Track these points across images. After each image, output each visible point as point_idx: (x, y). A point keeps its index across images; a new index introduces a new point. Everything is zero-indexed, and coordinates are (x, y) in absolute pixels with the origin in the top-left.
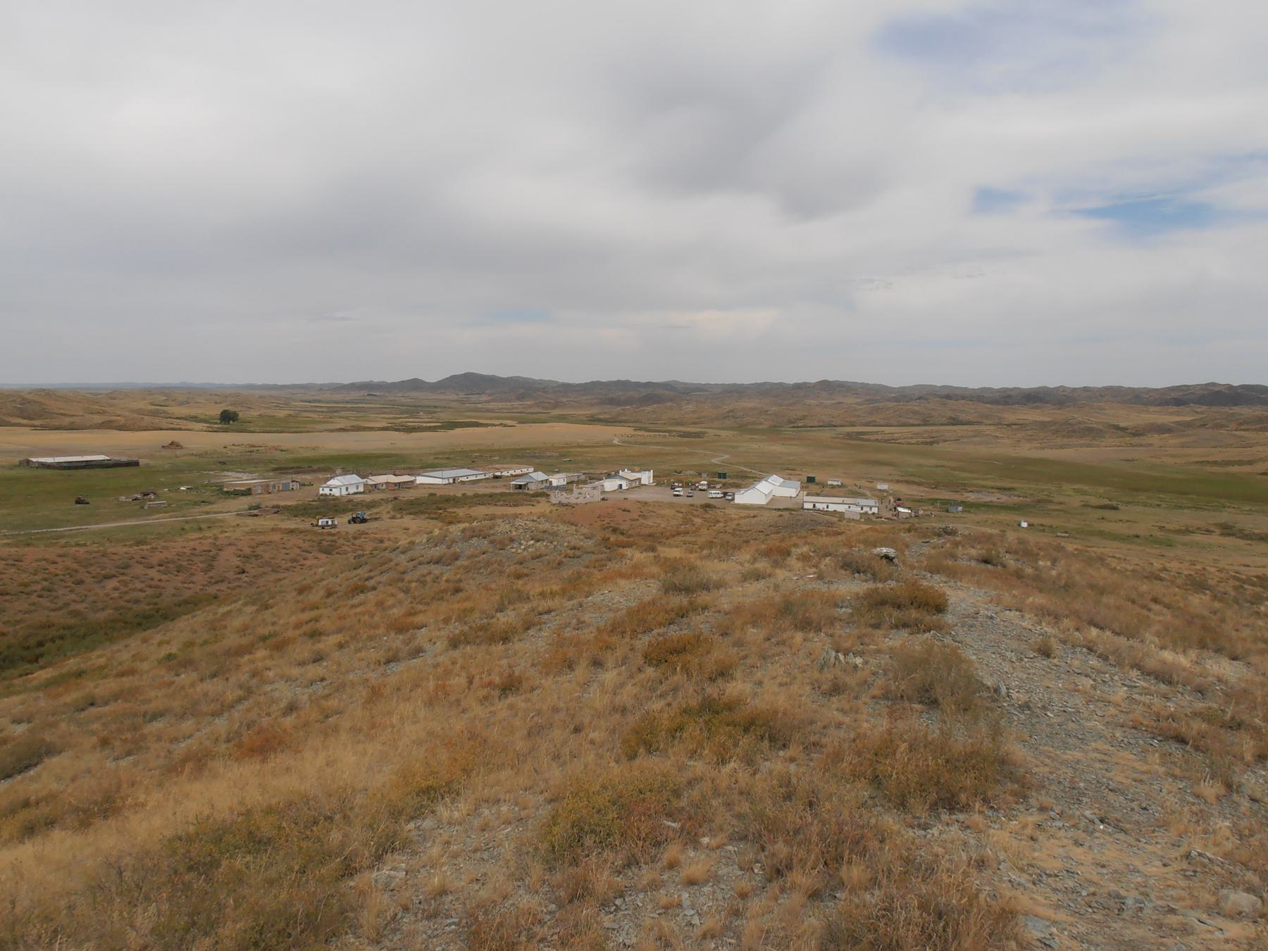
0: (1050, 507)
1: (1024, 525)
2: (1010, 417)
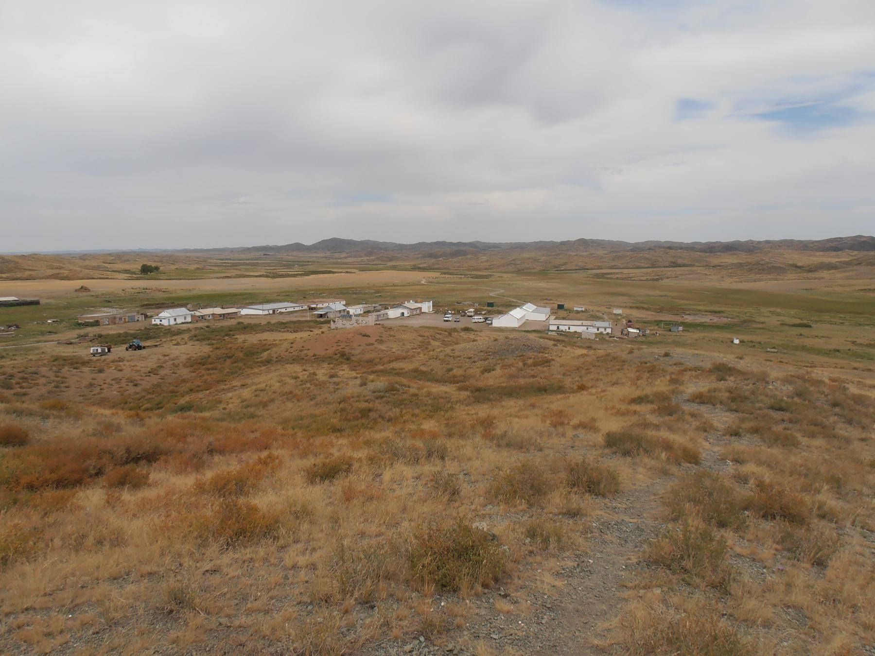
0: (754, 326)
1: (737, 341)
2: (715, 261)
